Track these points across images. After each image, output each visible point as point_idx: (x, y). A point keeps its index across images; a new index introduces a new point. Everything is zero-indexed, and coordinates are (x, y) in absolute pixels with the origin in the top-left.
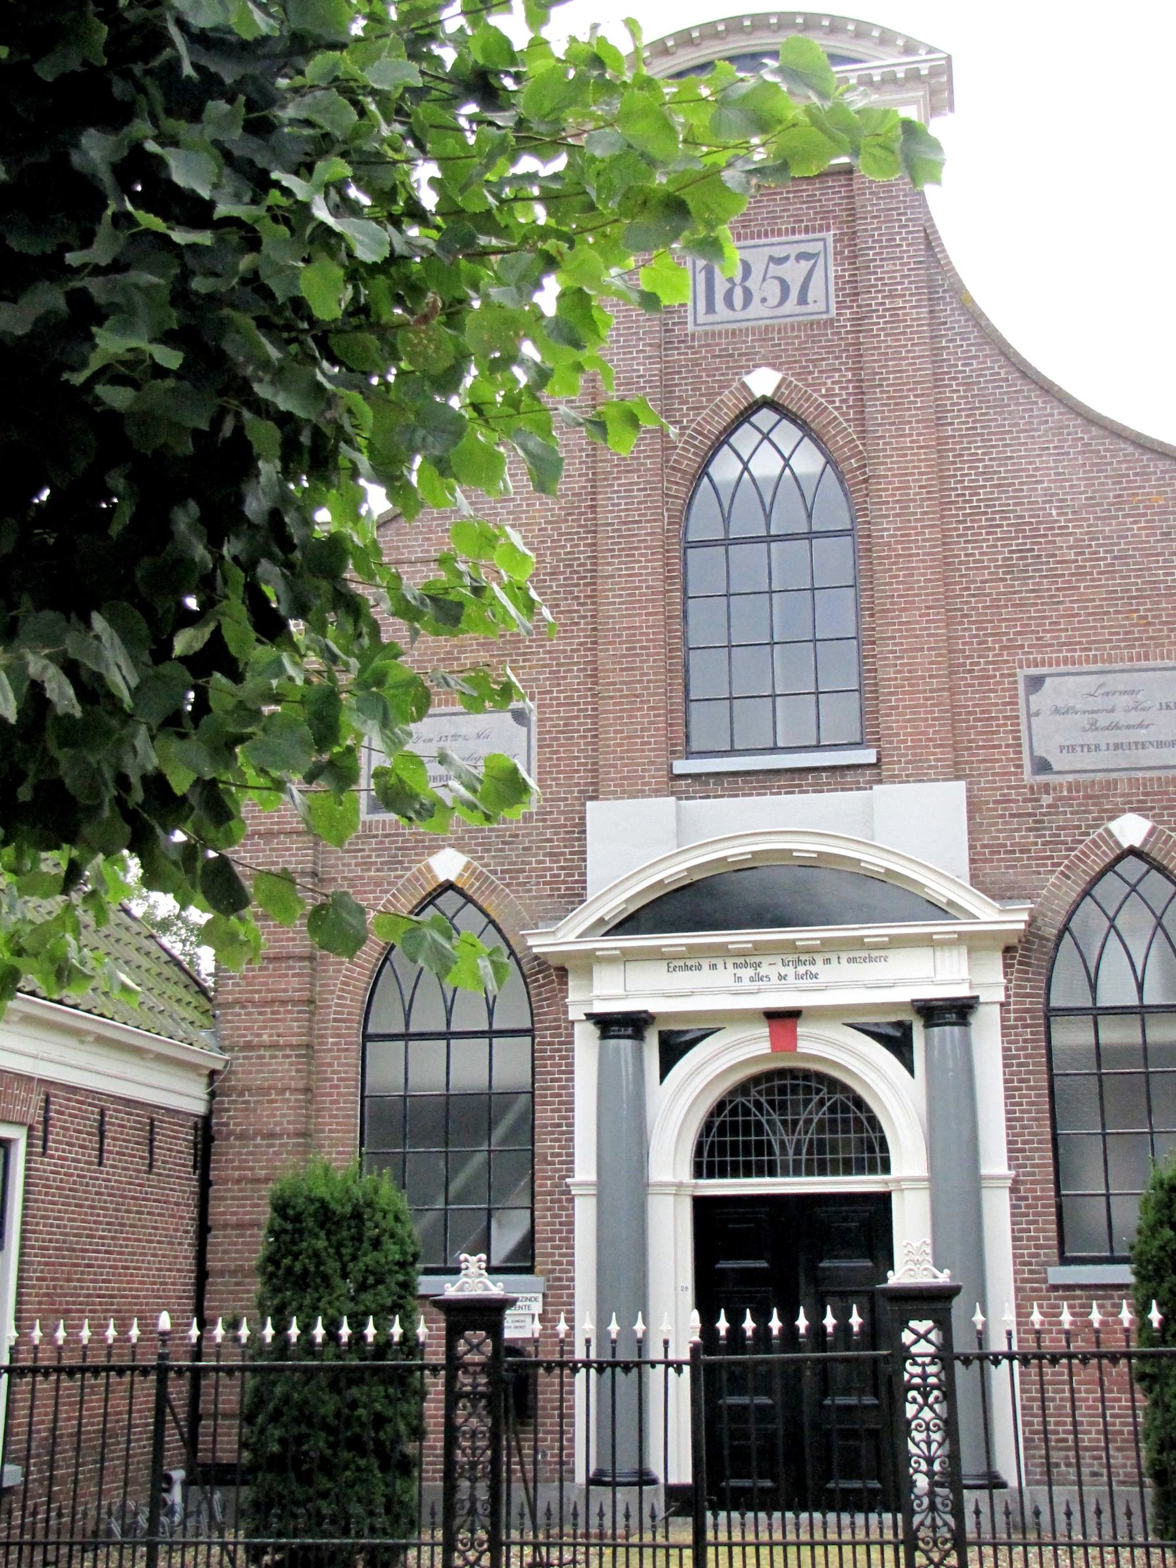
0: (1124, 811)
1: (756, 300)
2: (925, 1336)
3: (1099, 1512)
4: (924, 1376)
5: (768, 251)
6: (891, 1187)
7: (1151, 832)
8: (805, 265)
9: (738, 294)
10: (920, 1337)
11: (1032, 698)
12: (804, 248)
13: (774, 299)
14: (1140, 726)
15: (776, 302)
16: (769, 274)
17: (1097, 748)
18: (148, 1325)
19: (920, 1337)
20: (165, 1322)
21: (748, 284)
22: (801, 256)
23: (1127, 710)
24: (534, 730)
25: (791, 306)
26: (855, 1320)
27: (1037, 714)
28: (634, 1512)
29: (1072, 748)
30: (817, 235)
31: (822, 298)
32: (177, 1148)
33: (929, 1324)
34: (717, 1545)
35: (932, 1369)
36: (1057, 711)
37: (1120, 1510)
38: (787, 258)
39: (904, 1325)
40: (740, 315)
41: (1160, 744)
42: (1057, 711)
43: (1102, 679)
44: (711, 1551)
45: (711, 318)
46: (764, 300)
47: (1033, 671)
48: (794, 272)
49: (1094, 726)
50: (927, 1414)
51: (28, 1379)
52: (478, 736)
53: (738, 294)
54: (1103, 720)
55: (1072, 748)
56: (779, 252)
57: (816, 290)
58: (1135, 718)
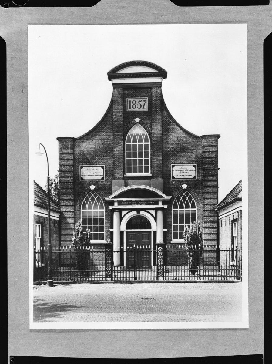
0: (184, 184)
1: (137, 107)
2: (161, 249)
3: (225, 267)
4: (160, 253)
5: (139, 100)
6: (151, 231)
7: (187, 187)
8: (144, 102)
9: (134, 106)
10: (160, 249)
11: (173, 168)
12: (144, 100)
13: (139, 107)
14: (187, 173)
15: (140, 107)
16: (139, 103)
17: (181, 175)
18: (133, 247)
19: (160, 249)
20: (134, 246)
21: (136, 104)
22: (143, 101)
23: (185, 171)
24: (84, 166)
25: (142, 109)
26: (195, 247)
27: (173, 170)
28: (226, 266)
29: (178, 175)
30: (146, 98)
31: (146, 108)
32: (56, 224)
33: (161, 247)
34: (202, 270)
35: (161, 252)
36: (176, 170)
37: (224, 266)
38: (141, 101)
39: (162, 248)
40: (134, 109)
41: (189, 175)
42: (176, 170)
43: (182, 166)
44: (136, 273)
45: (130, 109)
46: (138, 107)
47: (173, 165)
48: (142, 103)
49: (181, 173)
50: (160, 257)
51: (101, 253)
52: (96, 170)
53: (134, 106)
54: (182, 172)
55: (178, 175)
56: (140, 100)
57: (146, 107)
58: (186, 172)
